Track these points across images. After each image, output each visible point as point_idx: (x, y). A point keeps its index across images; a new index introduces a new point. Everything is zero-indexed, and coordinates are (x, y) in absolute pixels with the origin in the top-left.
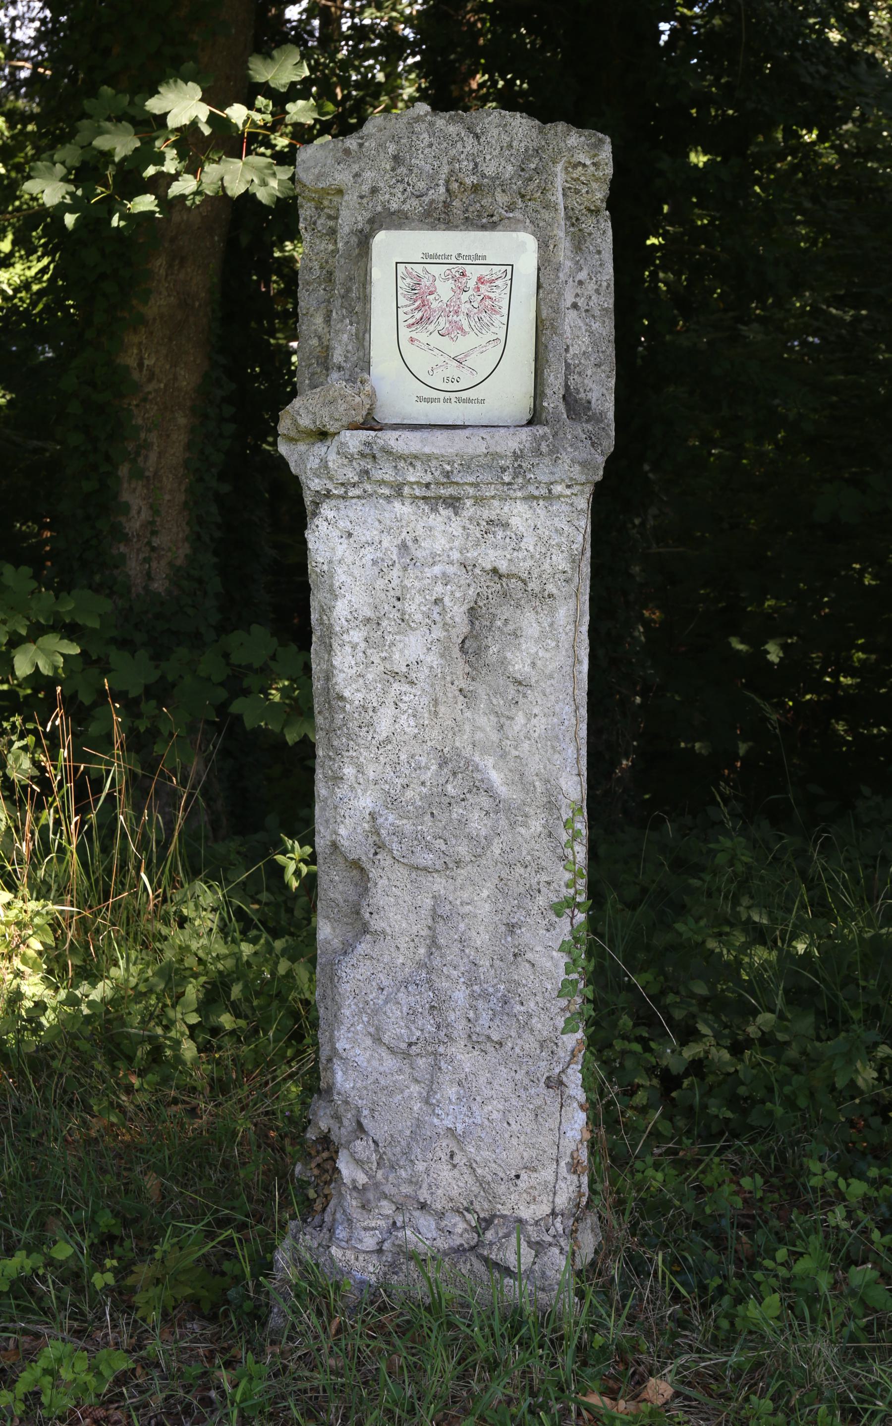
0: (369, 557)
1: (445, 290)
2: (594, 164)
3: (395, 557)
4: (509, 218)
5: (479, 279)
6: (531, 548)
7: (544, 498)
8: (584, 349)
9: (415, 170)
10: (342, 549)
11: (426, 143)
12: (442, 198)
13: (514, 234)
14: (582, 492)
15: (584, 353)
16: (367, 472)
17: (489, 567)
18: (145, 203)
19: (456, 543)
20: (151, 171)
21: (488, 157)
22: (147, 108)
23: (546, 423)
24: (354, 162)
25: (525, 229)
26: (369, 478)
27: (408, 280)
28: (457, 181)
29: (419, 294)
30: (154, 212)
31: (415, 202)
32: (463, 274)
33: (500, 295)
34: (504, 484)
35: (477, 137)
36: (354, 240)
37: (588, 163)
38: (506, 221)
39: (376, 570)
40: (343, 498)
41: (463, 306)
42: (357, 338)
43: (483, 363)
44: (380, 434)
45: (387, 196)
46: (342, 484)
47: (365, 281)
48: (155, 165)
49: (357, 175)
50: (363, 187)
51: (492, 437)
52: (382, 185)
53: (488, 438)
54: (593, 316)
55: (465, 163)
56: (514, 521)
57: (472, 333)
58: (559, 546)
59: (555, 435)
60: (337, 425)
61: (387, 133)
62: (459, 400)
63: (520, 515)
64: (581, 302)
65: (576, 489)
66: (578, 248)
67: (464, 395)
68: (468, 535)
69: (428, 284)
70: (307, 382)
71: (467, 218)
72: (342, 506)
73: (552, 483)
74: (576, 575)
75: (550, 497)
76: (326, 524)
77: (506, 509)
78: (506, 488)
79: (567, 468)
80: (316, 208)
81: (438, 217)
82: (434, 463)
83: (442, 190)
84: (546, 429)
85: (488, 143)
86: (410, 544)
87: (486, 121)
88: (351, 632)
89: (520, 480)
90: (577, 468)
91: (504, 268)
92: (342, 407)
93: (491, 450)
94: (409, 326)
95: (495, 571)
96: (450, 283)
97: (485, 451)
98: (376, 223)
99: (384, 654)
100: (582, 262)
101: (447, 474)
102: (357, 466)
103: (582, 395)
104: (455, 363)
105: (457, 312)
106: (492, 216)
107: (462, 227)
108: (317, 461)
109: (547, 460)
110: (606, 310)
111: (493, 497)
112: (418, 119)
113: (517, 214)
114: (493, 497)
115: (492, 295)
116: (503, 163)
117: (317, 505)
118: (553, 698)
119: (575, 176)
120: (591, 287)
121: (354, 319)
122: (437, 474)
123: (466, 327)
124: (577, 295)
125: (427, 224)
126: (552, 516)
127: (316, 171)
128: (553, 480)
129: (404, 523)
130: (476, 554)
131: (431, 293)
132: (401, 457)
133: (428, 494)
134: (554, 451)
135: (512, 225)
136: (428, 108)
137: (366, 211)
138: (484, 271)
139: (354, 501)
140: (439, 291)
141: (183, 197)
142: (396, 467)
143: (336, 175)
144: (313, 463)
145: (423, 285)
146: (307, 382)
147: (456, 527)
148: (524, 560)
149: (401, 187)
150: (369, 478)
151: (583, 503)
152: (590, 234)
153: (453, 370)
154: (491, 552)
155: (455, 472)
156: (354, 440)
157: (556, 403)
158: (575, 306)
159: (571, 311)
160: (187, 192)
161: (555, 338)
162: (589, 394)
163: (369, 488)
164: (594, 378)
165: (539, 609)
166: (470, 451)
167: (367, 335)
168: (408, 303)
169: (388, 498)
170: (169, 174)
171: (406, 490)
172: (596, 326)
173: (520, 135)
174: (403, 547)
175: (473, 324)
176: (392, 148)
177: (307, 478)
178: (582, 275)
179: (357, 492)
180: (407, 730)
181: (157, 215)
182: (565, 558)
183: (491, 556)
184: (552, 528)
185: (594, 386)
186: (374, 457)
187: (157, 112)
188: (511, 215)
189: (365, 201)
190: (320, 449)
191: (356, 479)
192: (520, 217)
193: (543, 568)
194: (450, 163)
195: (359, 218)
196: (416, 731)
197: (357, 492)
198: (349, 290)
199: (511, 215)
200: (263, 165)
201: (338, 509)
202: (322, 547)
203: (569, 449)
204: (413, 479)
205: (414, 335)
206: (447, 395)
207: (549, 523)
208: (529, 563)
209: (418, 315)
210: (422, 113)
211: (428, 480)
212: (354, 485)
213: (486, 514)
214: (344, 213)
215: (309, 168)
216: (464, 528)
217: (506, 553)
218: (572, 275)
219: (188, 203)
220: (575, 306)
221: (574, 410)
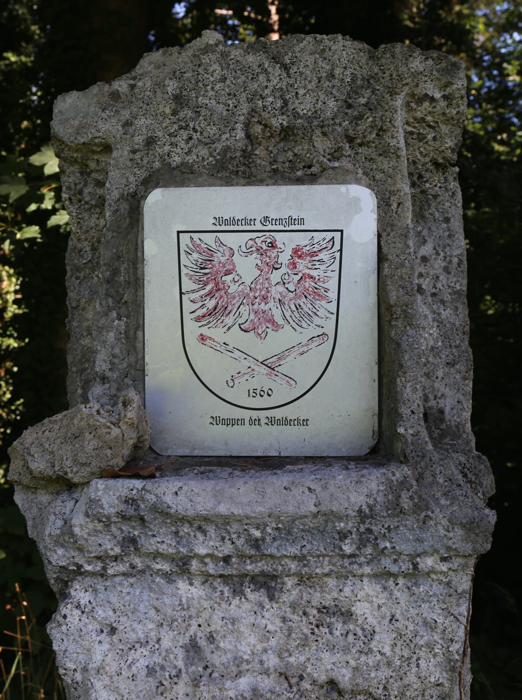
0: (143, 663)
1: (247, 268)
2: (445, 97)
3: (180, 664)
4: (333, 168)
6: (387, 650)
7: (405, 576)
8: (431, 343)
9: (203, 112)
10: (101, 651)
11: (217, 75)
12: (240, 145)
13: (343, 188)
14: (464, 567)
15: (433, 349)
16: (133, 541)
17: (323, 678)
18: (32, 232)
19: (273, 642)
20: (33, 207)
21: (301, 92)
22: (31, 162)
23: (404, 460)
24: (124, 108)
25: (358, 182)
26: (136, 549)
27: (195, 256)
28: (259, 122)
29: (209, 273)
30: (36, 238)
31: (204, 152)
32: (273, 245)
33: (325, 273)
34: (343, 556)
35: (286, 68)
36: (125, 207)
37: (438, 95)
38: (330, 172)
39: (152, 682)
40: (102, 576)
41: (273, 290)
42: (127, 338)
43: (304, 368)
44: (149, 484)
45: (167, 148)
46: (98, 558)
47: (136, 260)
48: (36, 203)
49: (127, 124)
50: (137, 139)
51: (325, 488)
52: (160, 134)
53: (319, 489)
54: (443, 302)
55: (271, 99)
56: (360, 609)
57: (287, 327)
58: (430, 646)
59: (420, 478)
60: (85, 471)
61: (167, 70)
62: (271, 421)
63: (367, 600)
65: (456, 562)
66: (420, 216)
67: (278, 414)
68: (290, 630)
69: (223, 259)
70: (79, 391)
71: (275, 171)
72: (100, 587)
73: (419, 555)
74: (457, 688)
75: (415, 574)
76: (77, 612)
77: (347, 590)
78: (346, 562)
79: (442, 532)
80: (82, 173)
81: (235, 169)
82: (235, 527)
83: (240, 134)
84: (406, 470)
85: (301, 74)
86: (203, 643)
87: (297, 49)
89: (369, 550)
90: (459, 532)
91: (330, 235)
92: (90, 444)
93: (323, 508)
94: (198, 319)
95: (332, 684)
96: (254, 259)
97: (314, 509)
98: (150, 182)
100: (425, 232)
101: (256, 544)
102: (118, 533)
104: (264, 370)
105: (265, 299)
106: (310, 167)
107: (269, 181)
108: (59, 523)
109: (410, 521)
110: (458, 293)
111: (327, 575)
112: (207, 49)
113: (345, 163)
114: (327, 575)
116: (322, 97)
117: (66, 584)
119: (419, 115)
120: (439, 264)
121: (123, 311)
122: (240, 543)
123: (279, 320)
125: (221, 178)
126: (418, 601)
127: (77, 123)
128: (420, 550)
129: (193, 611)
130: (302, 659)
131: (228, 273)
132: (183, 520)
133: (228, 571)
134: (421, 506)
135: (341, 177)
136: (219, 37)
137: (140, 167)
138: (302, 240)
139: (117, 579)
140: (239, 269)
141: (58, 227)
142: (177, 533)
143: (101, 125)
144: (53, 527)
145: (216, 263)
146: (79, 391)
147: (271, 618)
148: (377, 667)
149: (184, 134)
150: (136, 549)
151: (464, 583)
152: (435, 197)
153: (262, 379)
154: (326, 656)
155: (268, 539)
156: (111, 495)
157: (417, 428)
160: (61, 223)
161: (410, 332)
162: (442, 402)
163: (138, 562)
164: (447, 381)
166: (291, 509)
167: (140, 333)
168: (196, 287)
169: (168, 577)
170: (47, 210)
171: (195, 565)
172: (446, 313)
173: (344, 61)
174: (193, 648)
175: (288, 314)
176: (172, 86)
177: (46, 547)
179: (122, 568)
181: (39, 240)
182: (440, 664)
184: (418, 619)
185: (447, 391)
186: (142, 519)
187: (37, 164)
188: (336, 164)
189: (138, 156)
190: (64, 505)
191: (117, 550)
192: (350, 166)
193: (406, 681)
194: (250, 100)
195: (132, 179)
197: (122, 568)
198: (115, 272)
199: (336, 164)
201: (95, 591)
202: (72, 648)
203: (443, 502)
204: (202, 551)
205: (205, 331)
206: (255, 414)
208: (385, 673)
209: (211, 304)
210: (211, 42)
211: (226, 552)
212: (116, 558)
213: (317, 598)
214: (114, 174)
215: (67, 120)
216: (284, 620)
217: (349, 658)
219: (62, 231)
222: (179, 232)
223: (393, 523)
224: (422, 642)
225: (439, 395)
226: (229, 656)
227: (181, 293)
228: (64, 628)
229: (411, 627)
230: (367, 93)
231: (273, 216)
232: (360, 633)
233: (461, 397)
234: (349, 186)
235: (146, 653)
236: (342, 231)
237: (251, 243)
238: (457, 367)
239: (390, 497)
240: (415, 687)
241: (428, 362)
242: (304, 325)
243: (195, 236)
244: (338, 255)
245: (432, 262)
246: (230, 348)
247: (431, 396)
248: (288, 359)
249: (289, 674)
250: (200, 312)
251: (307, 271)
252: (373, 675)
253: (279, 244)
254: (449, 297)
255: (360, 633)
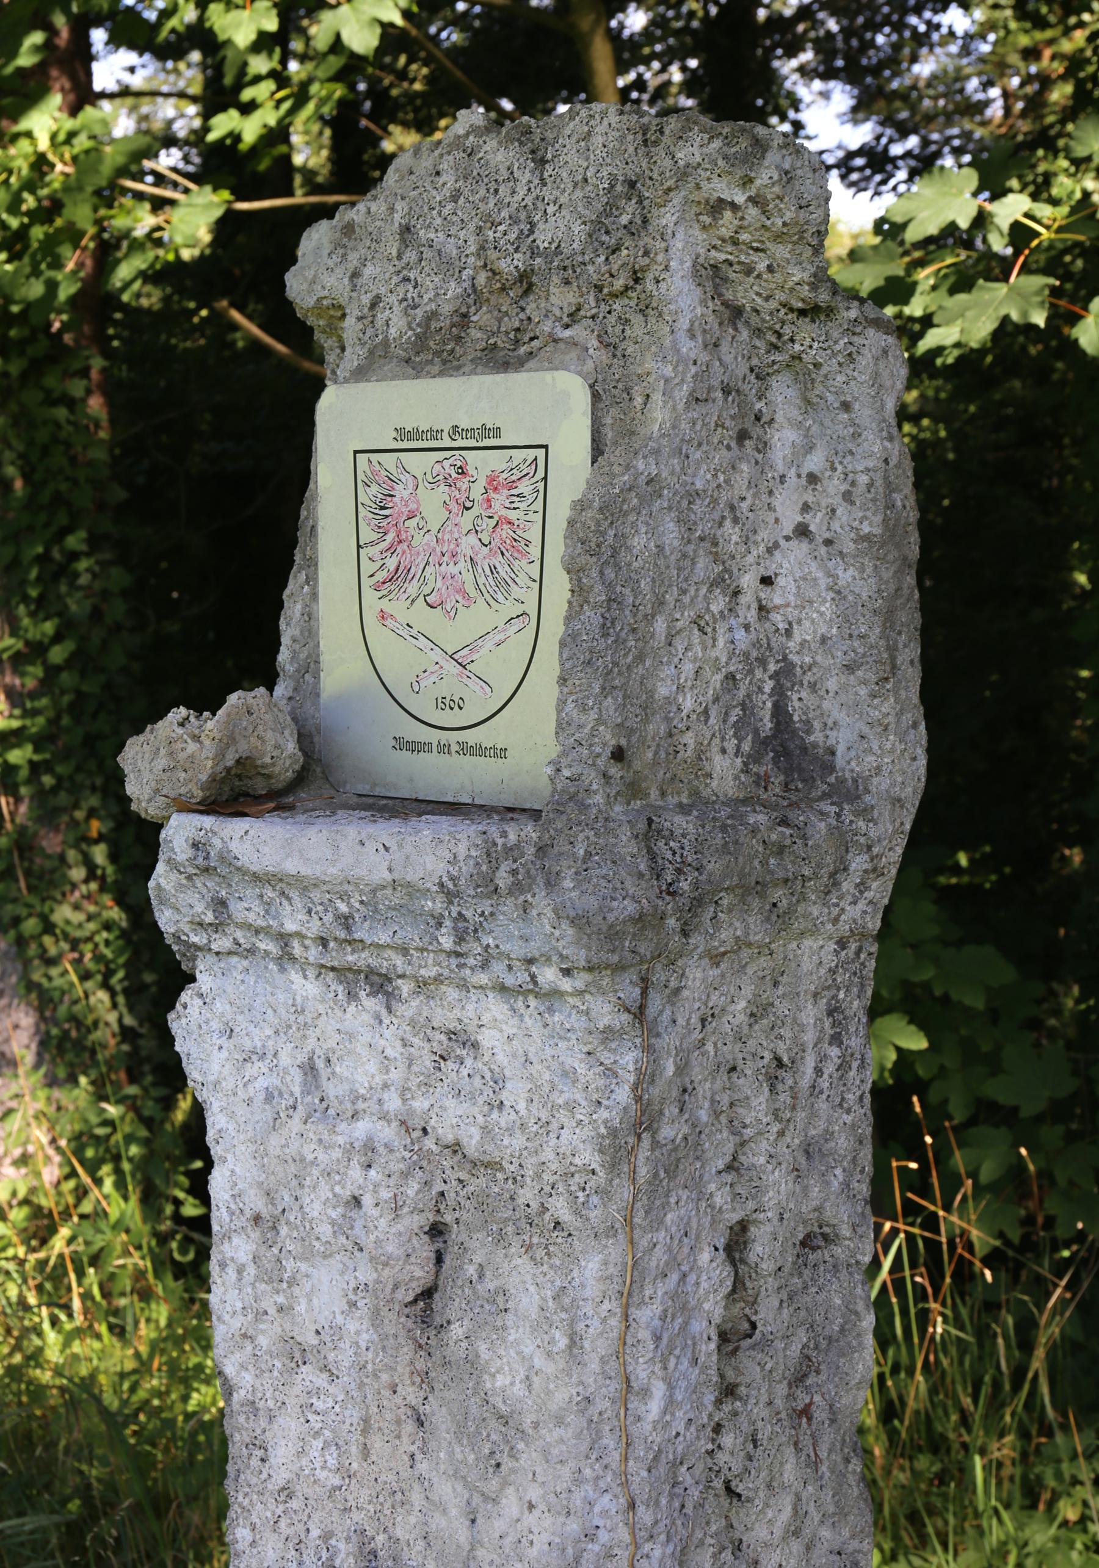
0: (261, 1083)
2: (753, 200)
5: (491, 480)
13: (548, 376)
15: (824, 640)
17: (450, 1138)
19: (395, 1075)
32: (462, 471)
37: (740, 199)
41: (464, 541)
51: (400, 846)
56: (487, 1038)
57: (481, 601)
62: (465, 749)
64: (816, 523)
67: (471, 737)
76: (200, 1002)
79: (548, 929)
86: (320, 1064)
88: (236, 1240)
91: (531, 453)
95: (455, 1148)
97: (388, 877)
99: (281, 1299)
101: (346, 921)
103: (817, 737)
104: (452, 668)
109: (509, 906)
115: (513, 515)
118: (566, 1472)
120: (834, 486)
124: (806, 508)
129: (309, 1017)
130: (426, 1105)
138: (495, 461)
148: (510, 1131)
158: (803, 531)
159: (794, 543)
162: (833, 734)
164: (843, 698)
165: (540, 1253)
168: (374, 536)
172: (846, 576)
175: (481, 580)
178: (815, 462)
180: (322, 1475)
183: (455, 1118)
184: (554, 1065)
185: (841, 716)
196: (337, 1482)
200: (1034, 289)
207: (549, 1052)
208: (518, 1142)
209: (392, 563)
216: (405, 1043)
218: (794, 461)
220: (803, 531)
221: (801, 770)
222: (356, 452)
223: (486, 906)
224: (560, 1101)
225: (830, 723)
226: (346, 1087)
227: (359, 546)
228: (184, 1021)
229: (547, 1076)
230: (631, 206)
231: (464, 425)
232: (488, 1076)
233: (866, 730)
234: (556, 374)
235: (265, 1070)
236: (546, 447)
237: (438, 467)
238: (860, 673)
239: (484, 868)
240: (553, 1167)
241: (815, 663)
242: (501, 598)
243: (374, 457)
244: (541, 485)
245: (825, 482)
246: (414, 632)
247: (817, 725)
248: (483, 651)
249: (410, 1123)
250: (381, 576)
251: (504, 512)
252: (506, 1142)
253: (470, 470)
254: (852, 545)
255: (488, 1076)
